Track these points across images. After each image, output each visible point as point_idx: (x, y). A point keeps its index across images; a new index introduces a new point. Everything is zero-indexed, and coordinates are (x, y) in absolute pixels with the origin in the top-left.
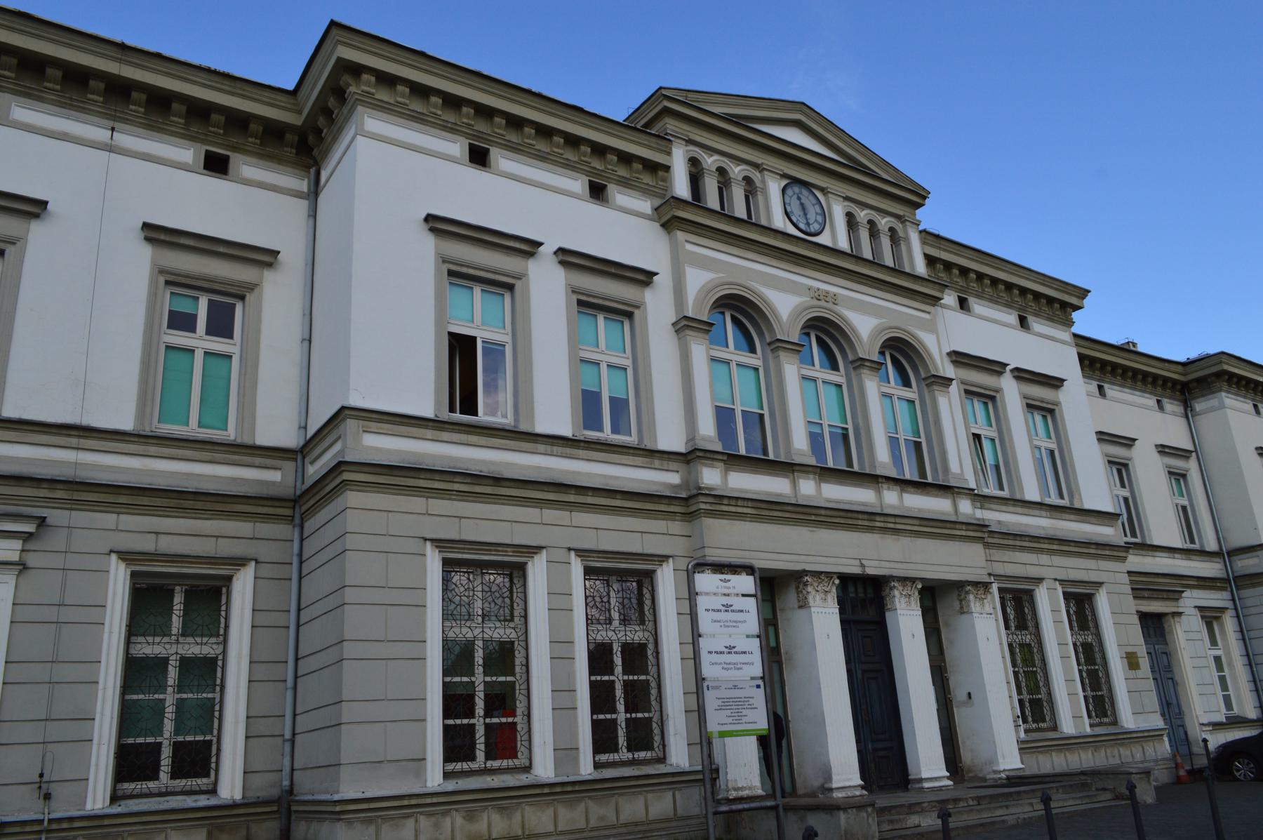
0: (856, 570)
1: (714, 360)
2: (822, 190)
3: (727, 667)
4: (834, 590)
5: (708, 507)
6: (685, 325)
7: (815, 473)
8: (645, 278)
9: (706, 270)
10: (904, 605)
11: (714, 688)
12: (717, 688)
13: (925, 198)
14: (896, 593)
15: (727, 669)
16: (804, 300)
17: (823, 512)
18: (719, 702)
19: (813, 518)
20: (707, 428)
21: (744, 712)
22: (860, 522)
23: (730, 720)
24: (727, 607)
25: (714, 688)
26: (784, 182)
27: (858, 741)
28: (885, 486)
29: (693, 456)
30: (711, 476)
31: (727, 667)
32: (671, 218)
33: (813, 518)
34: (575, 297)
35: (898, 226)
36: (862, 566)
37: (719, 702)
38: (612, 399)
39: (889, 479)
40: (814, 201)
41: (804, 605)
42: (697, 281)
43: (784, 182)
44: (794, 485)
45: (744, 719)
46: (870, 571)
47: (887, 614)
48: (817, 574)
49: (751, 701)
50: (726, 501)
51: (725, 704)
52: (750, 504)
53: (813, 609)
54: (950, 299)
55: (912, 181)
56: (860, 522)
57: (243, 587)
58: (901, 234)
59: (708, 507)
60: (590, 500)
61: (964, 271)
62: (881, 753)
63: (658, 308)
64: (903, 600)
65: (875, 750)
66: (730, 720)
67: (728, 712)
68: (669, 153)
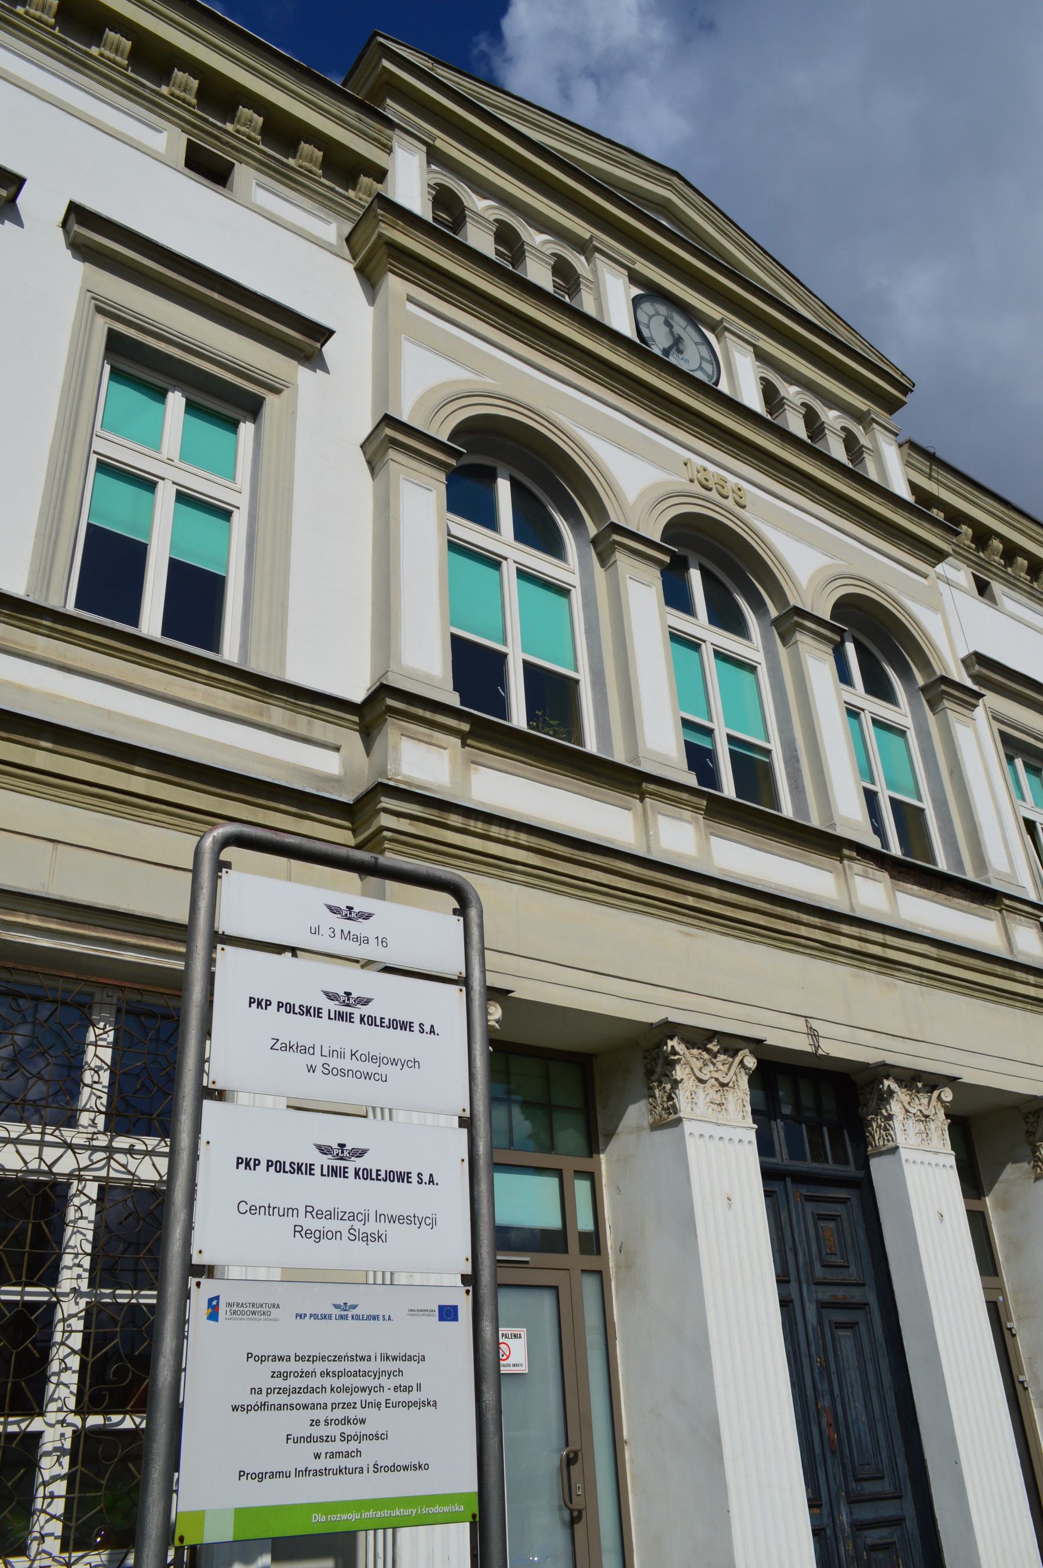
0: (801, 1043)
1: (456, 547)
2: (714, 326)
3: (314, 1225)
4: (744, 1081)
5: (404, 825)
6: (391, 437)
7: (696, 808)
8: (305, 339)
9: (450, 365)
10: (914, 1140)
11: (238, 1310)
12: (259, 1311)
13: (906, 390)
14: (895, 1107)
15: (319, 1236)
16: (680, 481)
17: (715, 892)
18: (261, 1375)
19: (690, 901)
20: (428, 668)
21: (376, 1420)
22: (804, 931)
23: (303, 1456)
24: (347, 1006)
25: (238, 1310)
26: (636, 291)
27: (814, 1503)
28: (857, 867)
29: (376, 712)
30: (424, 761)
31: (314, 1225)
32: (374, 261)
33: (690, 901)
34: (102, 325)
35: (858, 430)
36: (813, 1034)
37: (261, 1375)
38: (177, 570)
39: (864, 853)
40: (698, 339)
41: (668, 1120)
43: (636, 291)
44: (646, 825)
45: (372, 1452)
46: (831, 1048)
47: (875, 1164)
48: (699, 1038)
49: (412, 1373)
50: (455, 820)
51: (286, 1384)
52: (523, 838)
53: (687, 1126)
55: (882, 357)
56: (804, 931)
58: (863, 439)
59: (404, 825)
60: (41, 759)
61: (983, 536)
62: (874, 1536)
64: (913, 1127)
65: (859, 1526)
66: (303, 1456)
67: (299, 1423)
68: (388, 149)
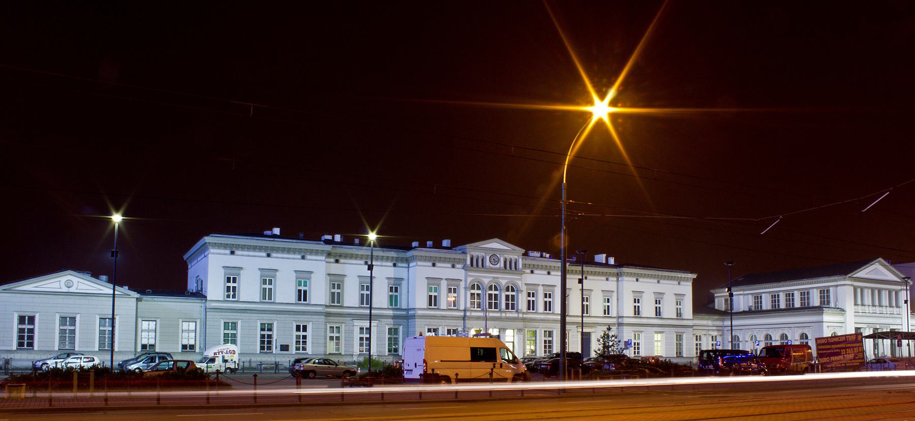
6: (466, 288)
42: (469, 279)
54: (528, 271)
57: (401, 328)
63: (462, 284)
